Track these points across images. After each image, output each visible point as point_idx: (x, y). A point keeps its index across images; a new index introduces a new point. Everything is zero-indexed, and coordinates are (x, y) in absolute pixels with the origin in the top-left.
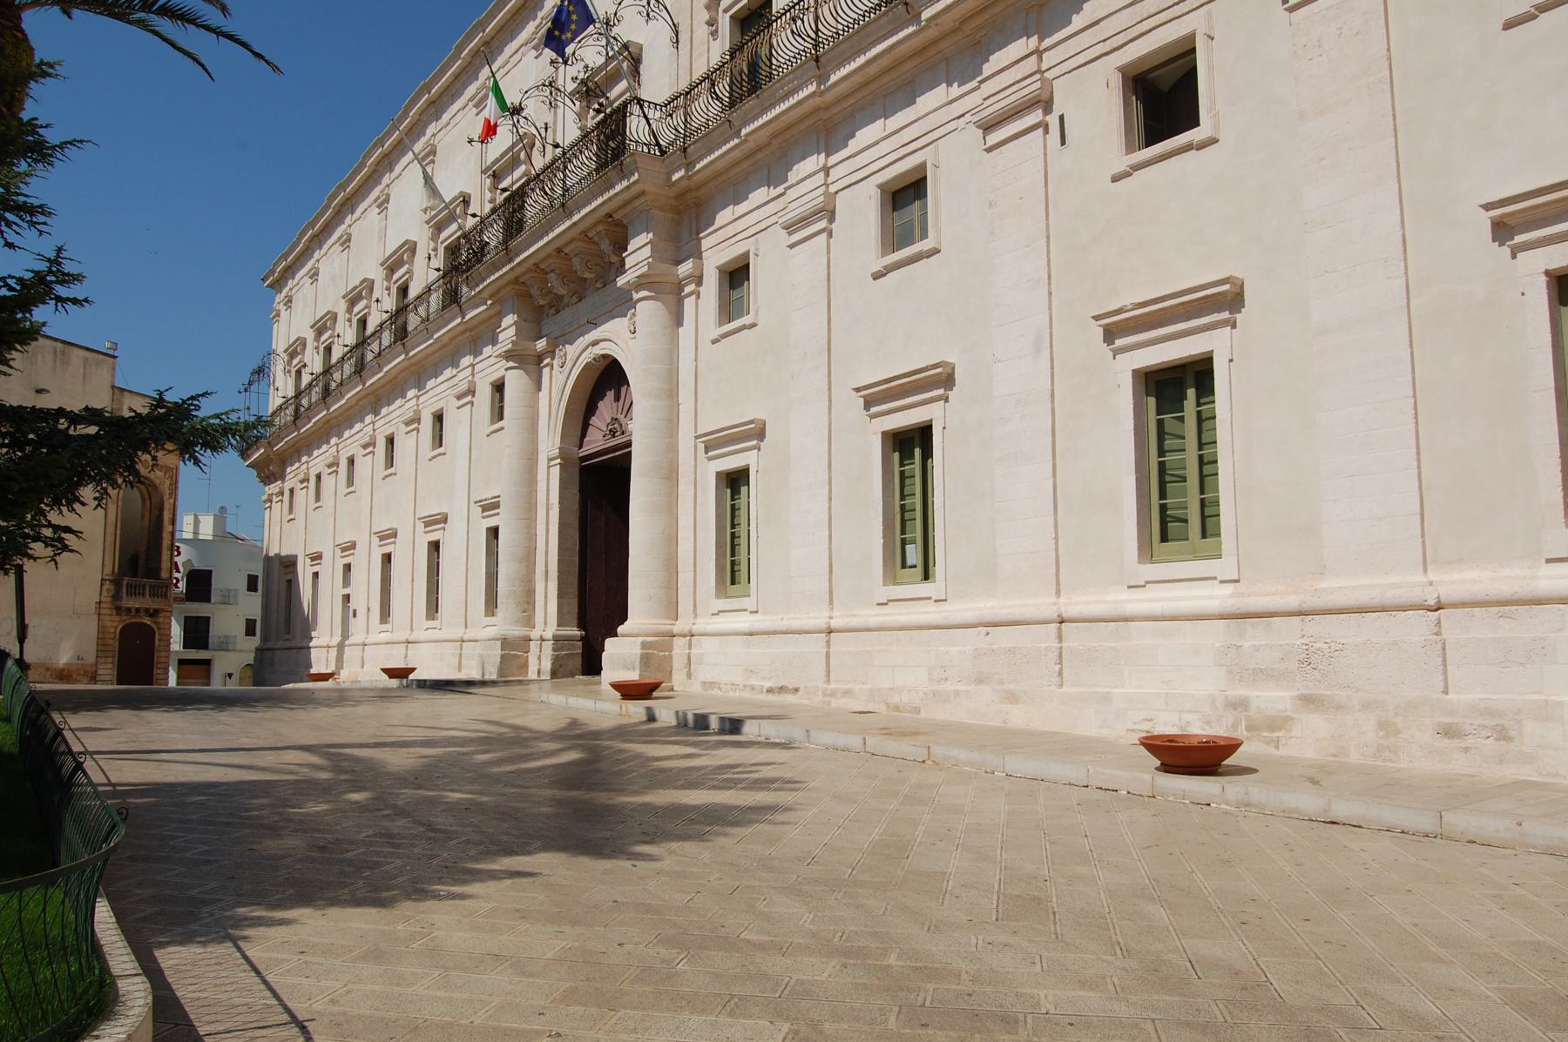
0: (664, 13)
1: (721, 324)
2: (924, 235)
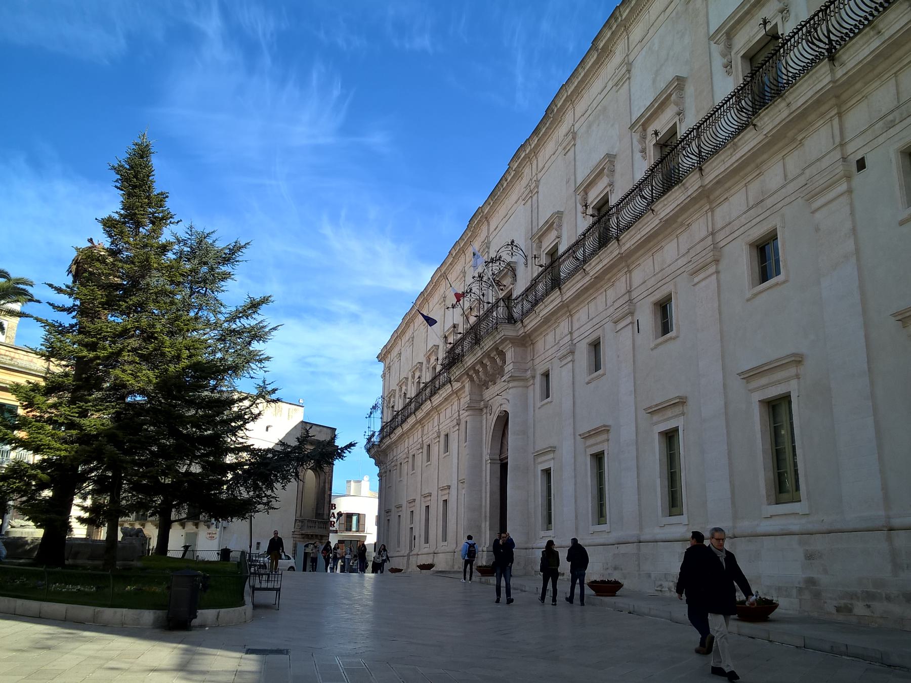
0: (521, 252)
1: (754, 286)
2: (778, 273)
